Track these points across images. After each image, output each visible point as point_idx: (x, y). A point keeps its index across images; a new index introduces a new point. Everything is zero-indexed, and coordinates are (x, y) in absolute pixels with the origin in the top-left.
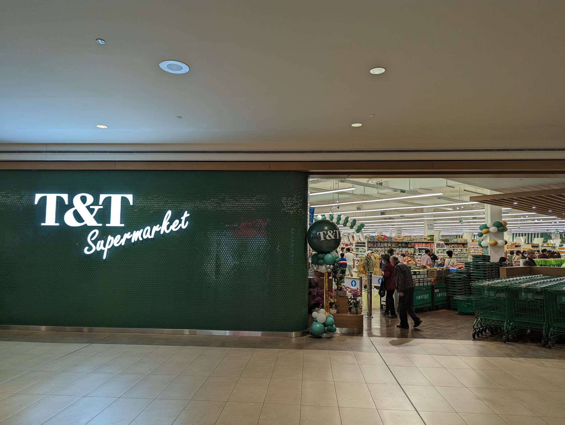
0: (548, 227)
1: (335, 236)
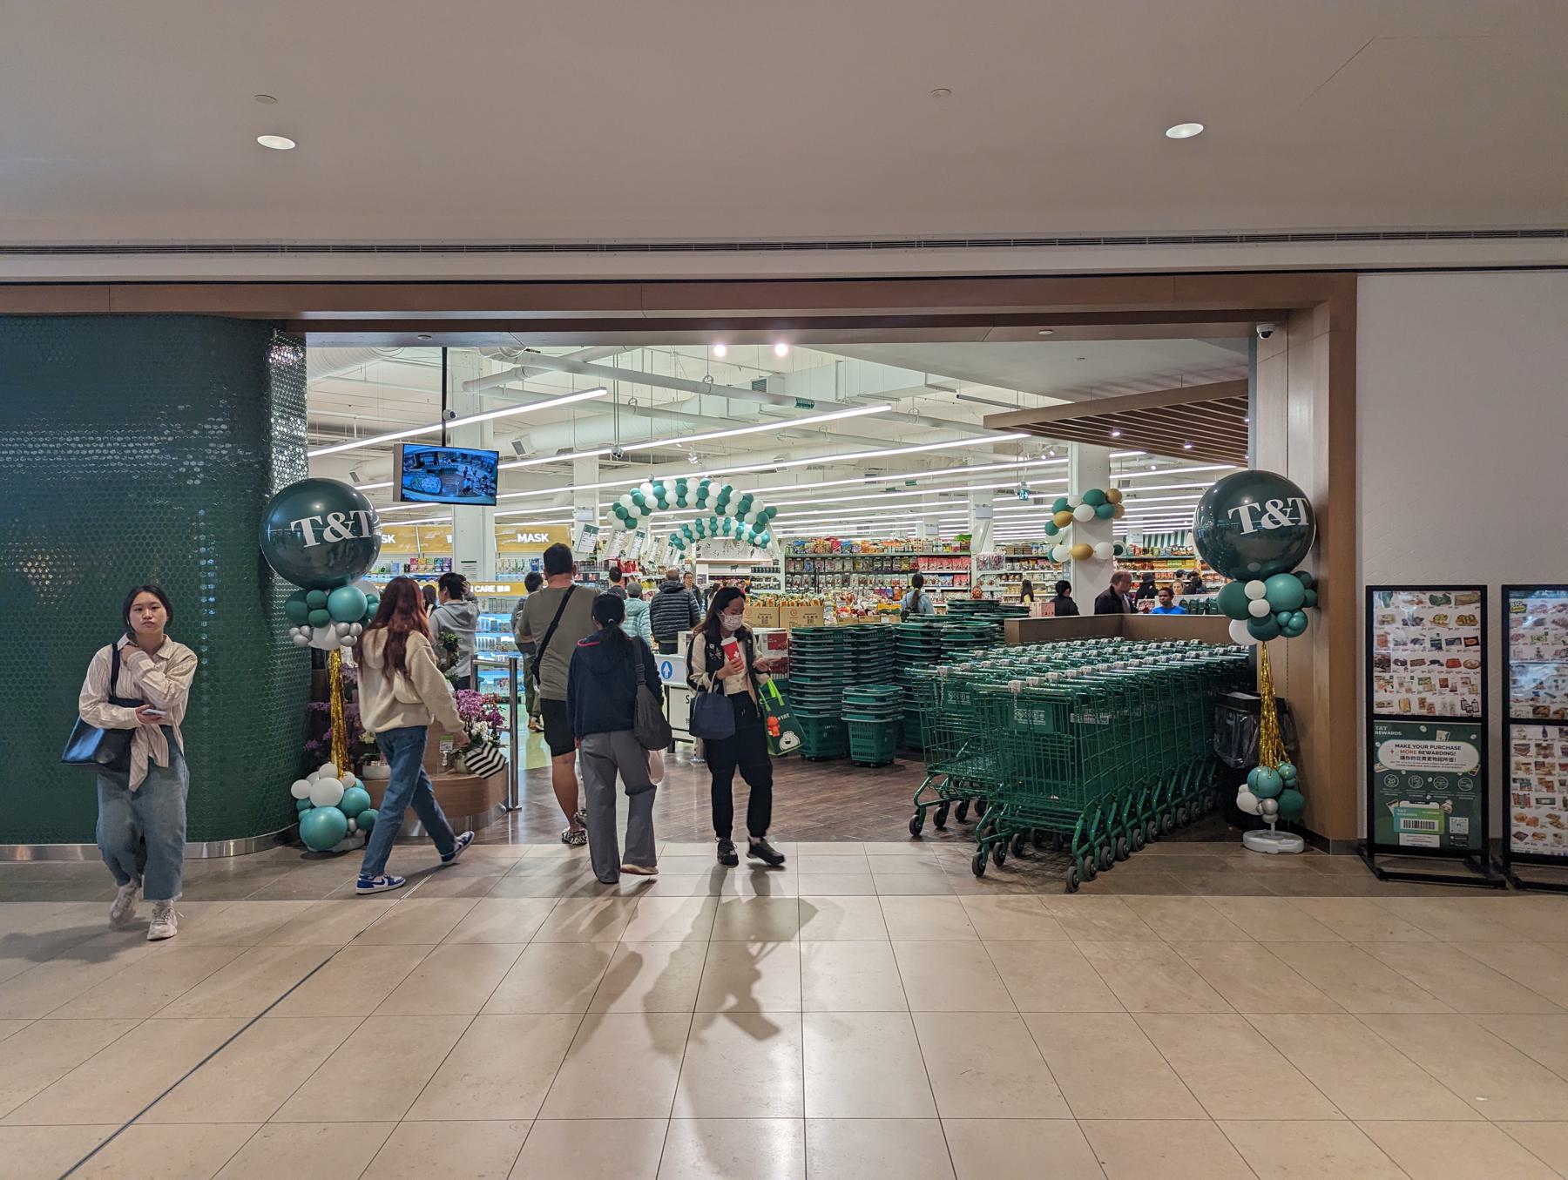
0: (951, 479)
1: (357, 527)
